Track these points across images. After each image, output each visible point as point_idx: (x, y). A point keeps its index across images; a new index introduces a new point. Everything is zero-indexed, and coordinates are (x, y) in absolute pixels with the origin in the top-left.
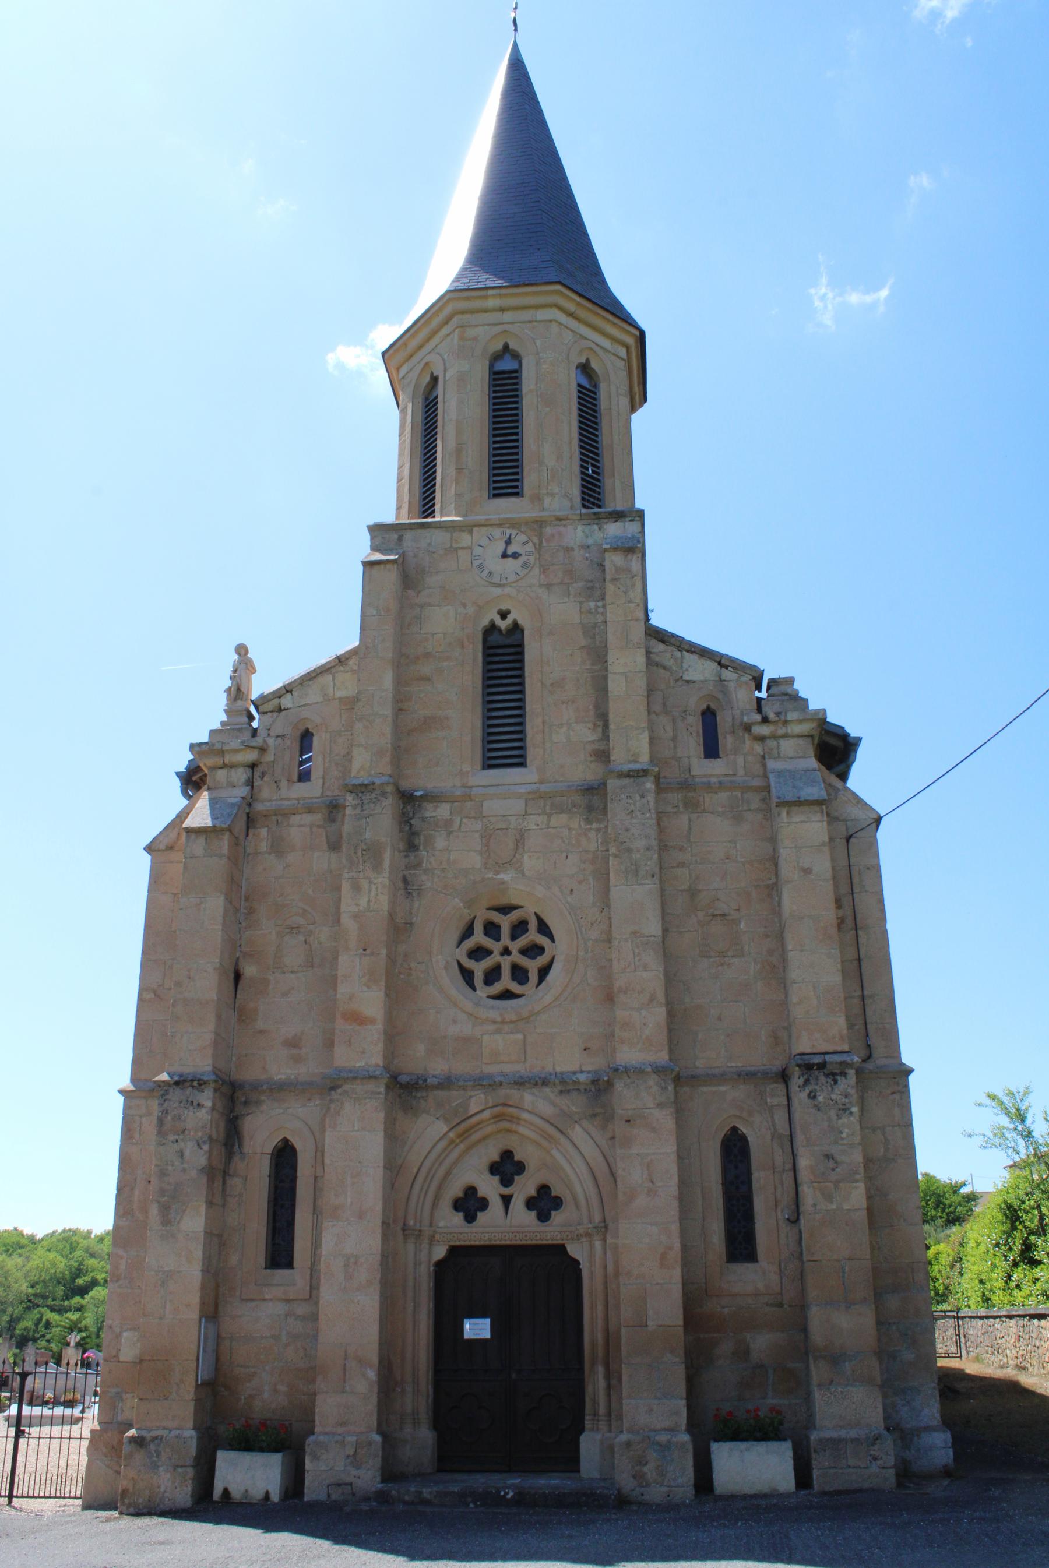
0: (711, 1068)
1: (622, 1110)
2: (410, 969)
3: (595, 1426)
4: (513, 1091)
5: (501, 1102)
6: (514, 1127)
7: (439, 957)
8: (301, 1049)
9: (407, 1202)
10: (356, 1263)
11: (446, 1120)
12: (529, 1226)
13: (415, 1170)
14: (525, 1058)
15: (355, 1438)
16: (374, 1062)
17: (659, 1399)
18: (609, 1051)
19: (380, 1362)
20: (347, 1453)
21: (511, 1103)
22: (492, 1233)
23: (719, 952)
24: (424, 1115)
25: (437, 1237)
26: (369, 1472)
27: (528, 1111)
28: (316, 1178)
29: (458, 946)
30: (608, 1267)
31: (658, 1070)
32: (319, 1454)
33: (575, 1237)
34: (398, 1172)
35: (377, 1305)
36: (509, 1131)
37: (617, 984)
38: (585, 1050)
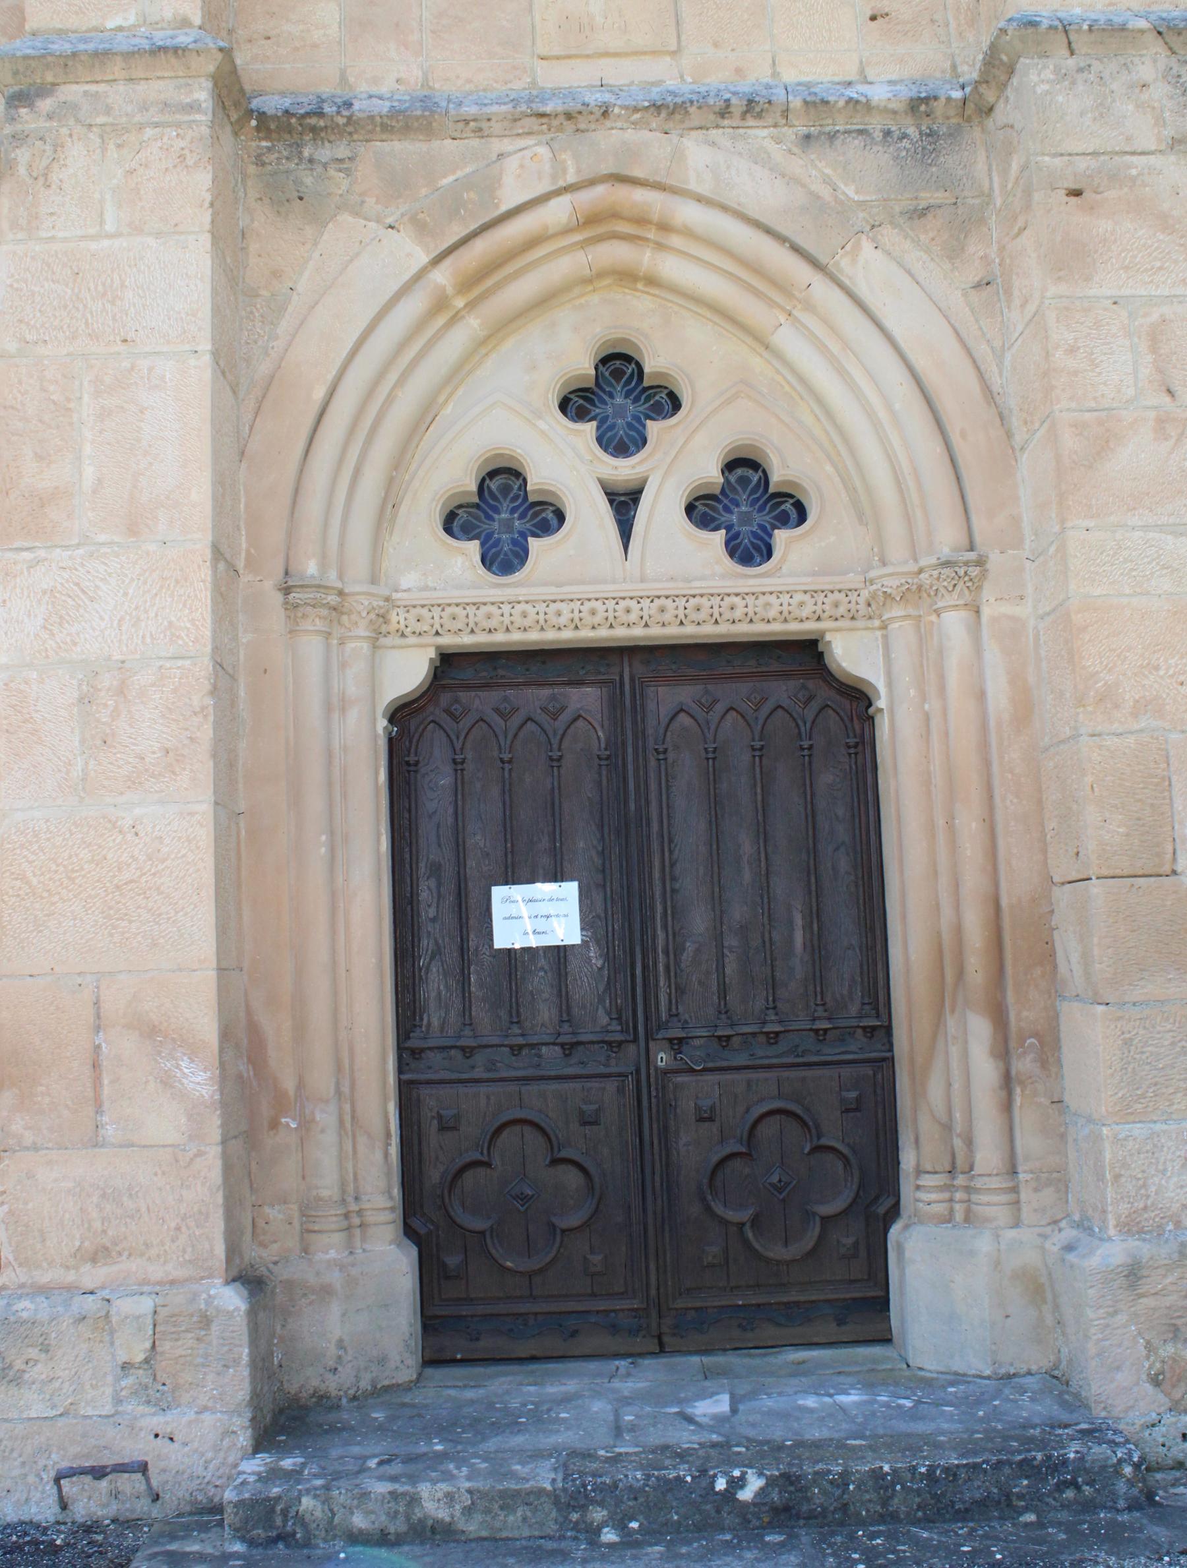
1: (1055, 155)
3: (957, 1207)
4: (645, 135)
5: (606, 168)
6: (646, 259)
9: (294, 503)
13: (319, 393)
14: (679, 42)
15: (146, 1305)
16: (168, 14)
18: (953, 24)
19: (225, 1035)
20: (122, 1357)
21: (638, 173)
24: (346, 218)
25: (397, 618)
26: (207, 1417)
27: (700, 199)
32: (19, 1364)
33: (863, 610)
35: (205, 836)
36: (627, 277)
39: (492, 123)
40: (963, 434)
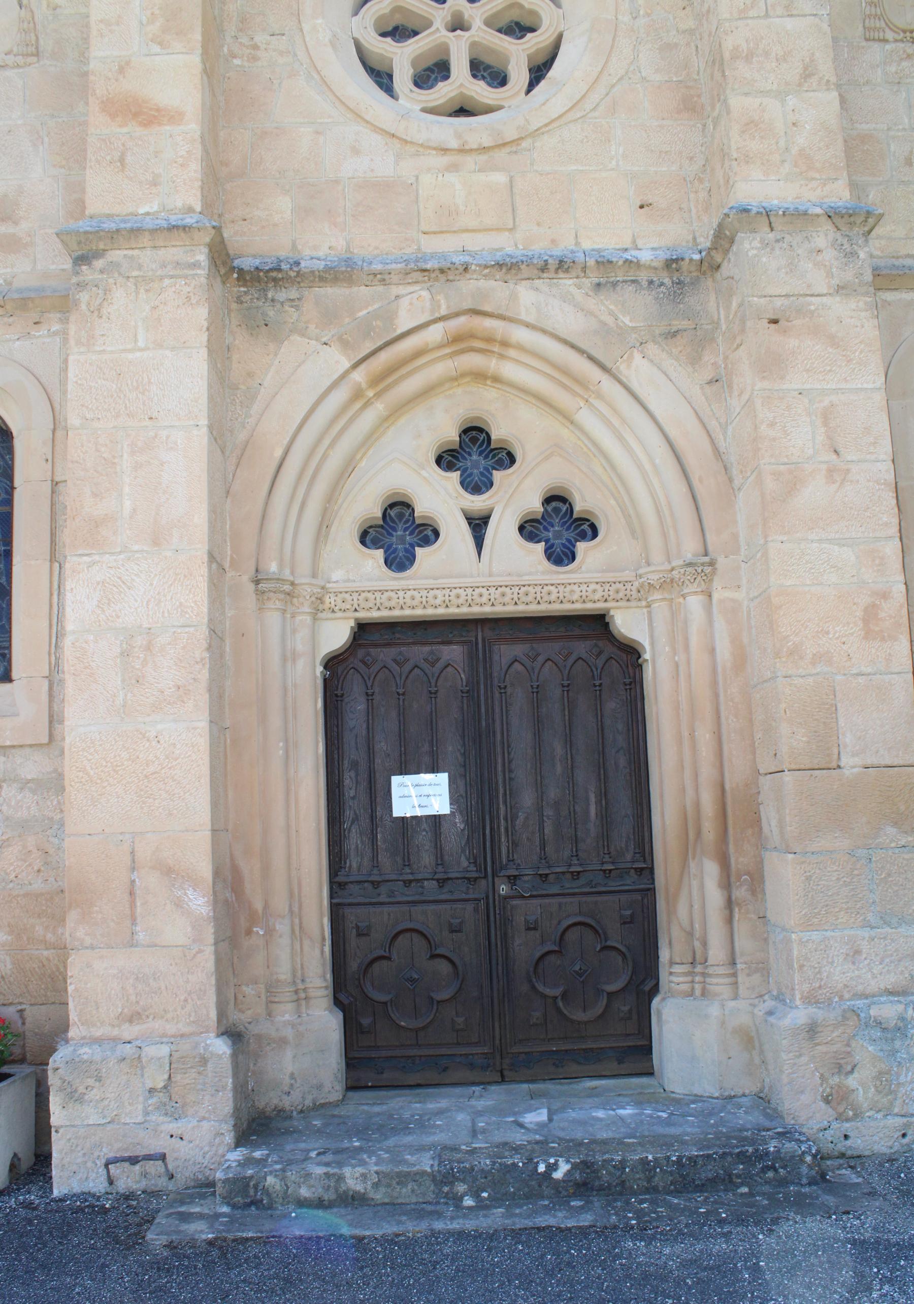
0: (898, 258)
1: (761, 297)
2: (256, 47)
4: (492, 283)
6: (492, 365)
7: (319, 21)
8: (16, 223)
10: (148, 648)
11: (345, 345)
12: (530, 574)
13: (278, 453)
15: (165, 1050)
16: (179, 204)
17: (872, 928)
21: (487, 308)
22: (451, 589)
23: (904, 31)
24: (296, 338)
25: (329, 600)
26: (205, 1124)
28: (55, 484)
29: (356, 13)
30: (718, 650)
31: (832, 215)
34: (240, 459)
36: (480, 376)
37: (729, 44)
38: (642, 207)
39: (392, 276)
40: (701, 480)
